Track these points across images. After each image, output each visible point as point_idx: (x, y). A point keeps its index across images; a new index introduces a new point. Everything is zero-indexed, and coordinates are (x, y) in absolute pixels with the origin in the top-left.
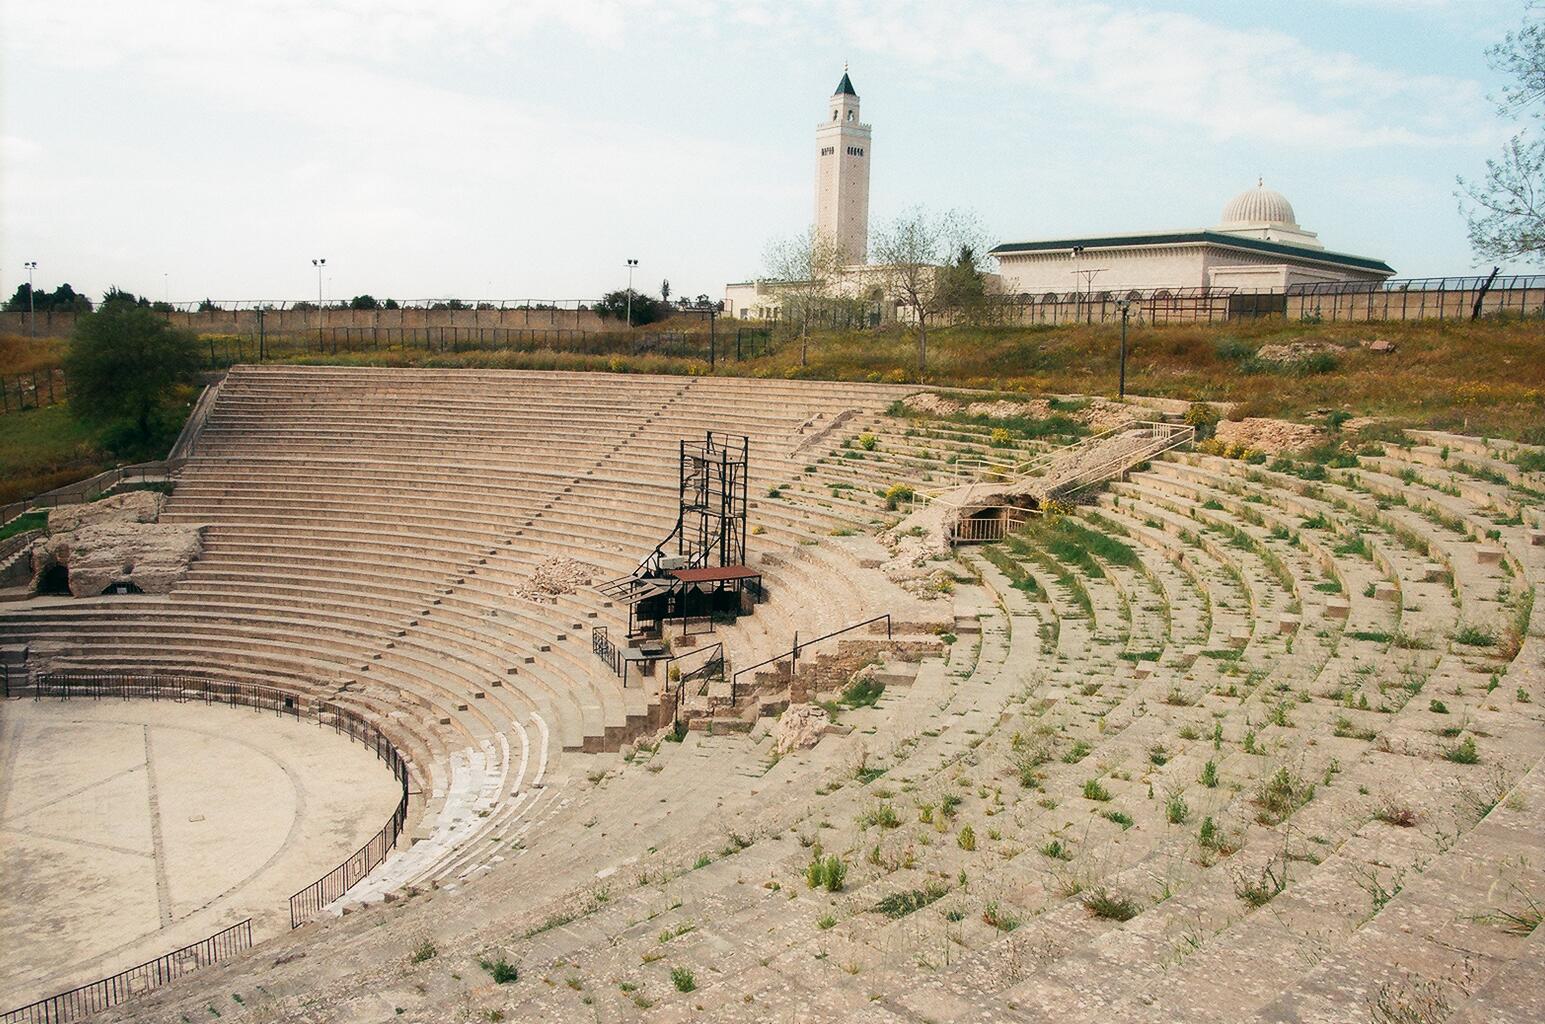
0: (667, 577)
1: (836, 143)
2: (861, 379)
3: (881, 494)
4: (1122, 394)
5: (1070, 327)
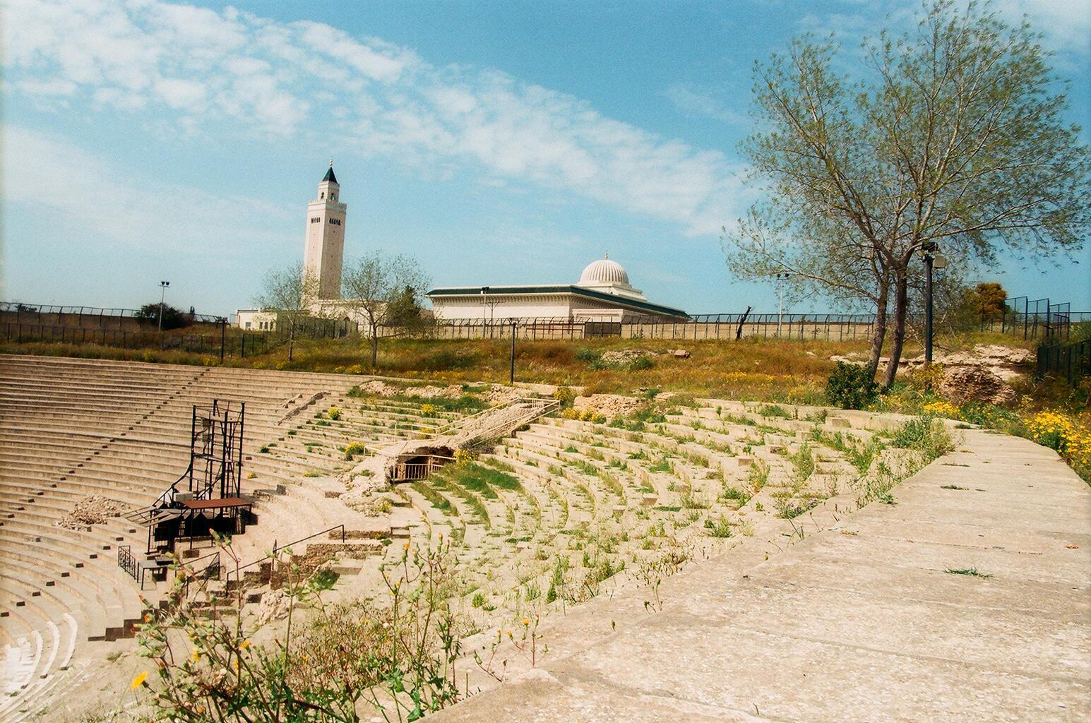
0: (179, 508)
1: (322, 215)
2: (331, 371)
3: (342, 450)
4: (512, 381)
5: (478, 340)
